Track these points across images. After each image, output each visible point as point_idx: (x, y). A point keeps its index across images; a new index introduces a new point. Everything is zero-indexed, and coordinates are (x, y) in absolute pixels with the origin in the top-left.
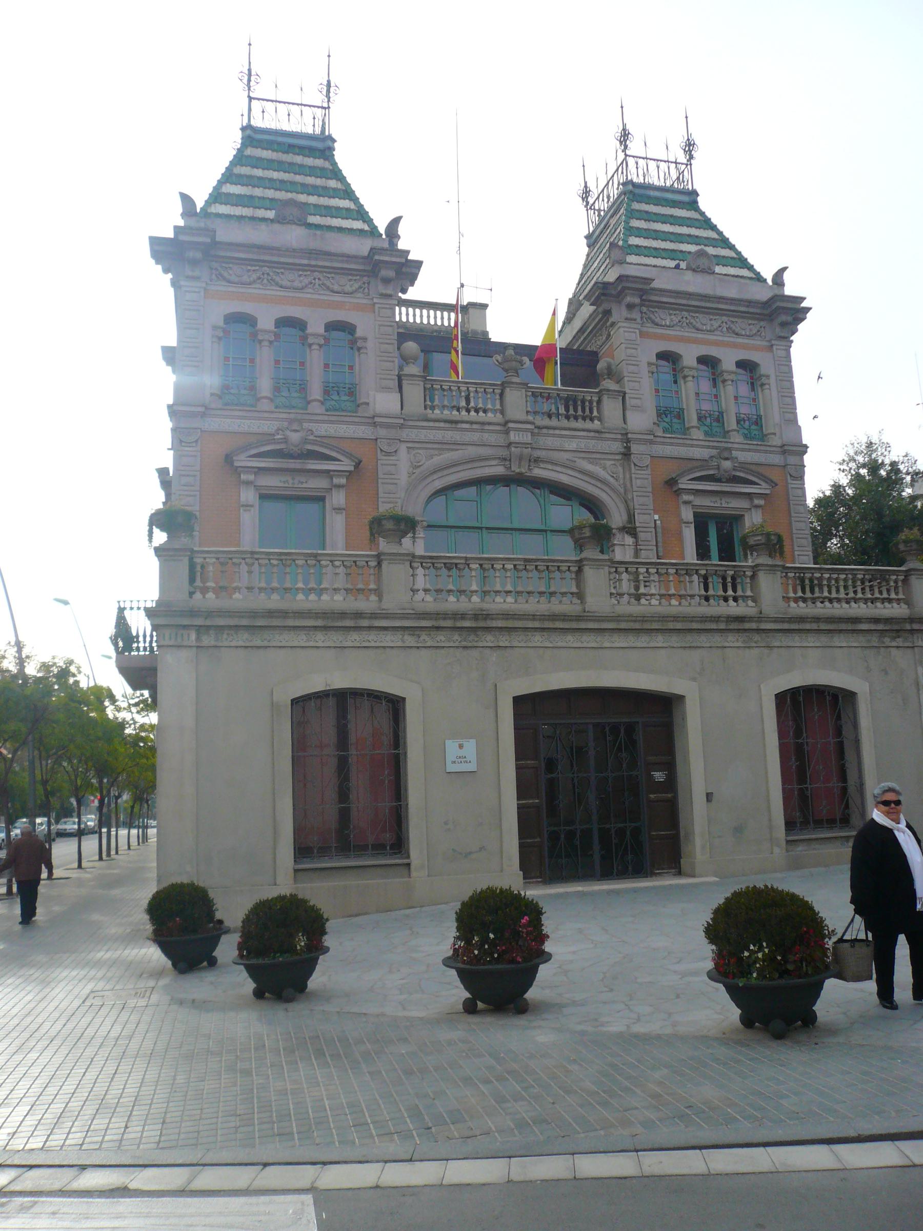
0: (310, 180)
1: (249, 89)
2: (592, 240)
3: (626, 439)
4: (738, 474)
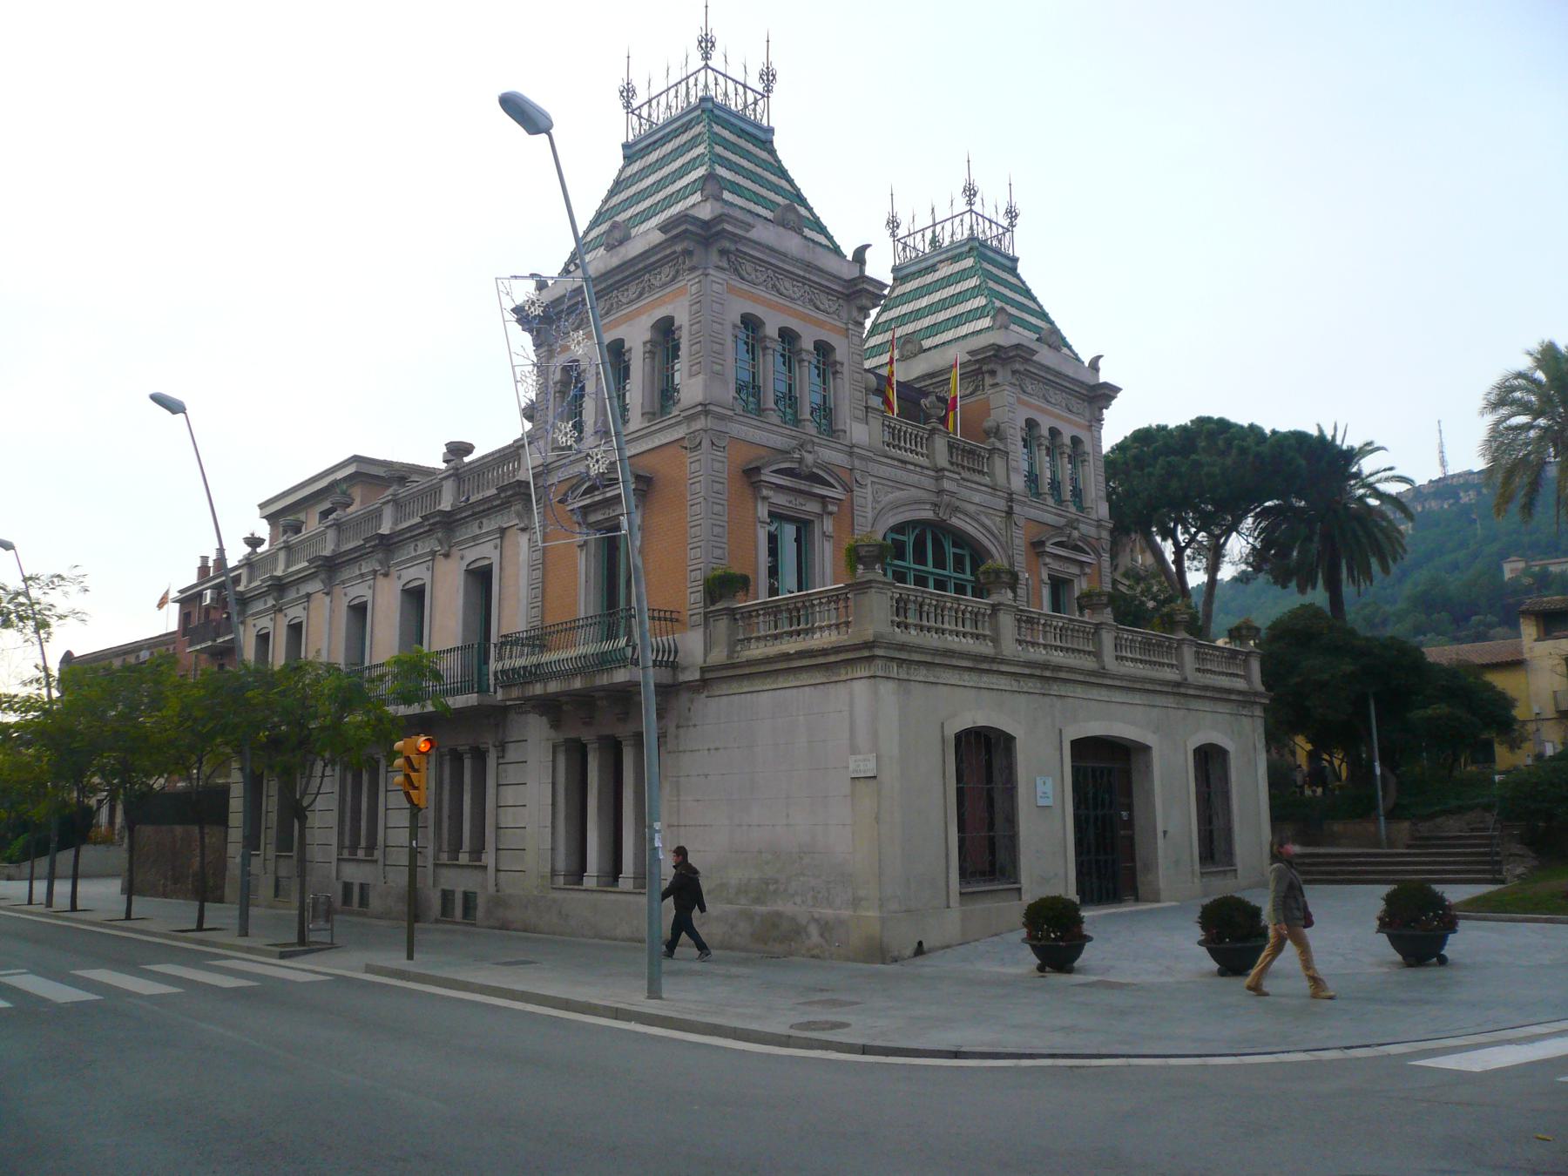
3: (1010, 498)
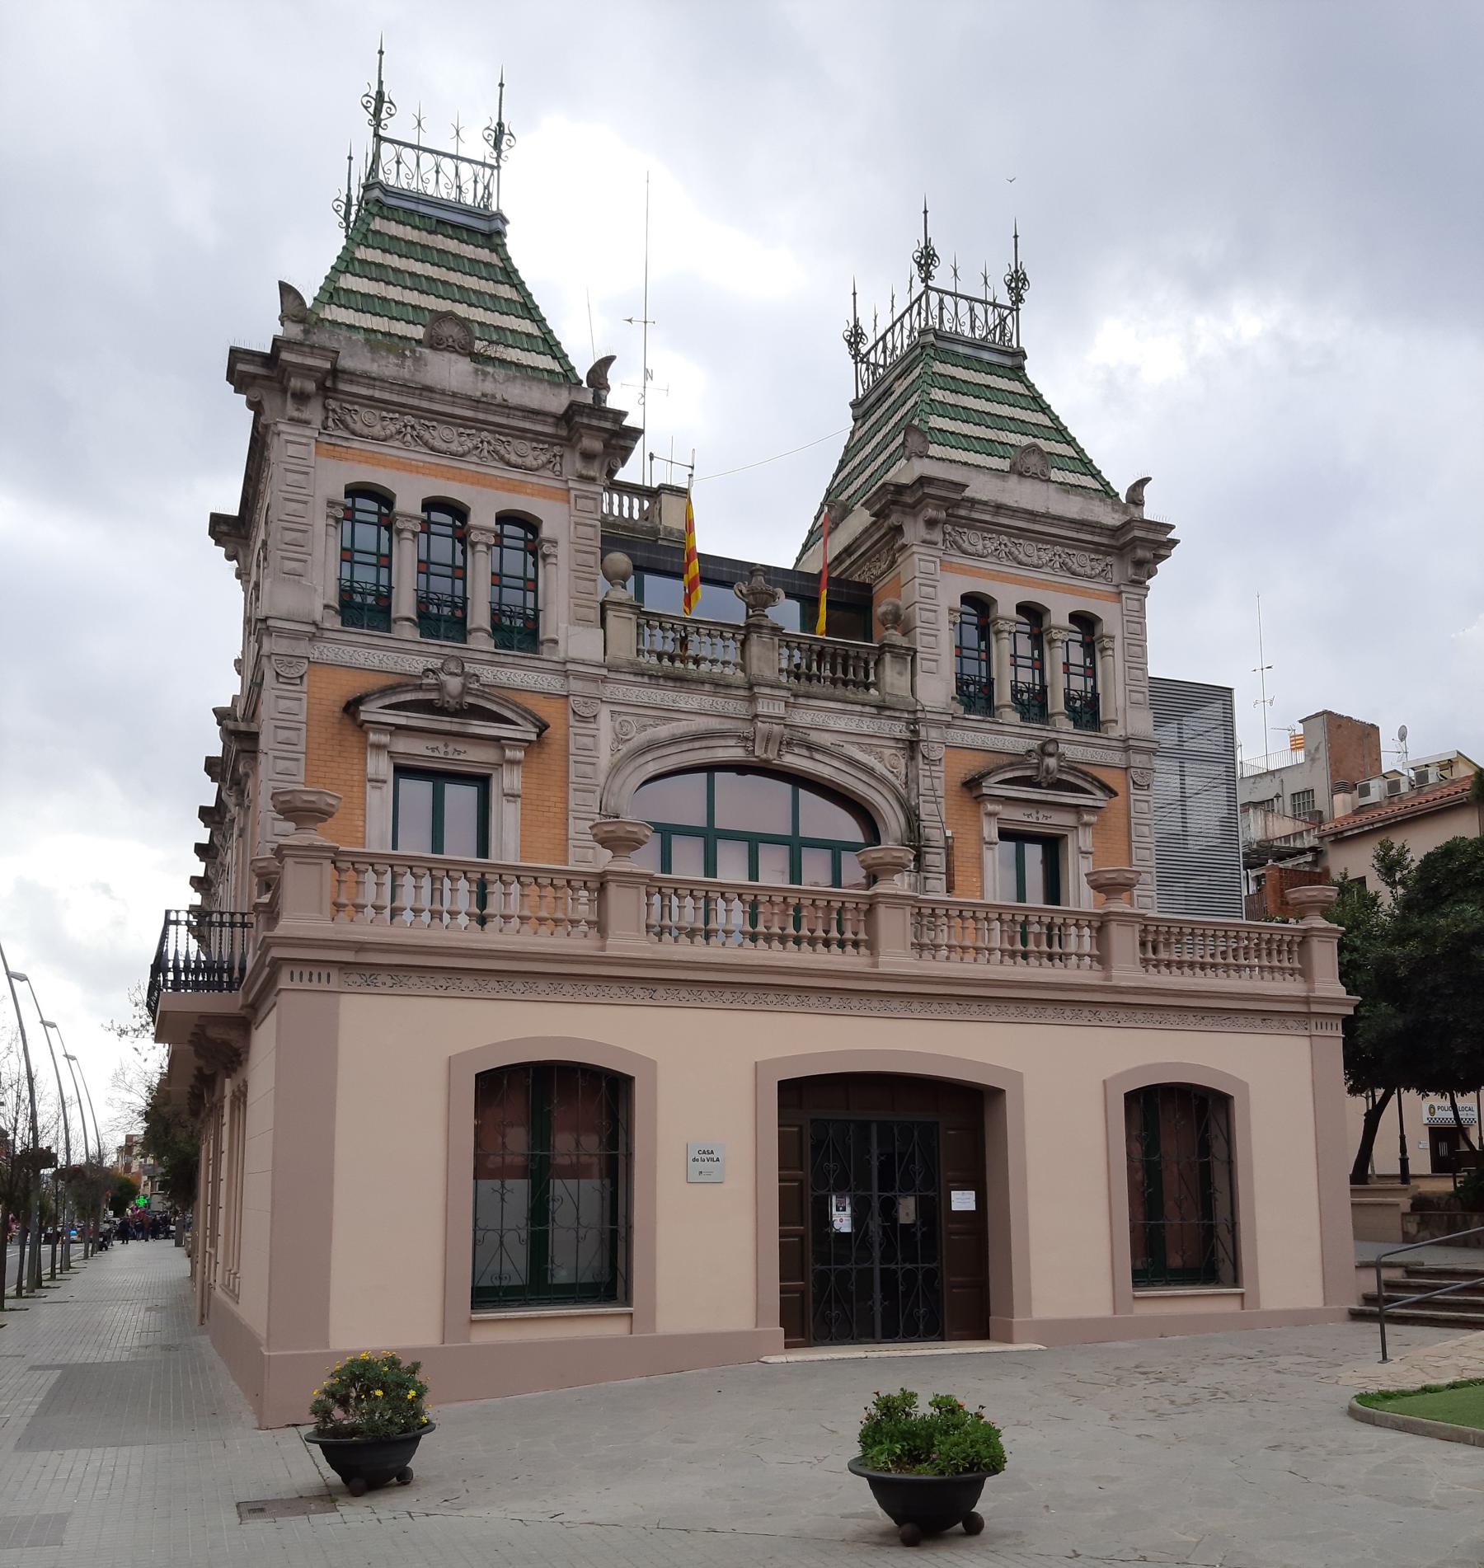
0: (471, 282)
1: (379, 125)
2: (862, 409)
4: (1064, 777)
